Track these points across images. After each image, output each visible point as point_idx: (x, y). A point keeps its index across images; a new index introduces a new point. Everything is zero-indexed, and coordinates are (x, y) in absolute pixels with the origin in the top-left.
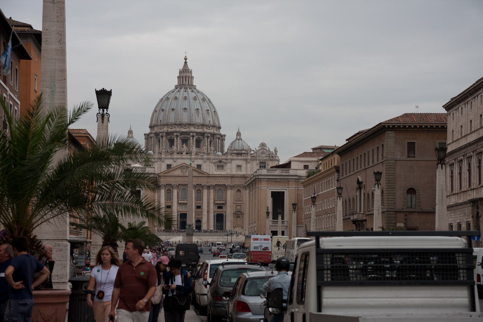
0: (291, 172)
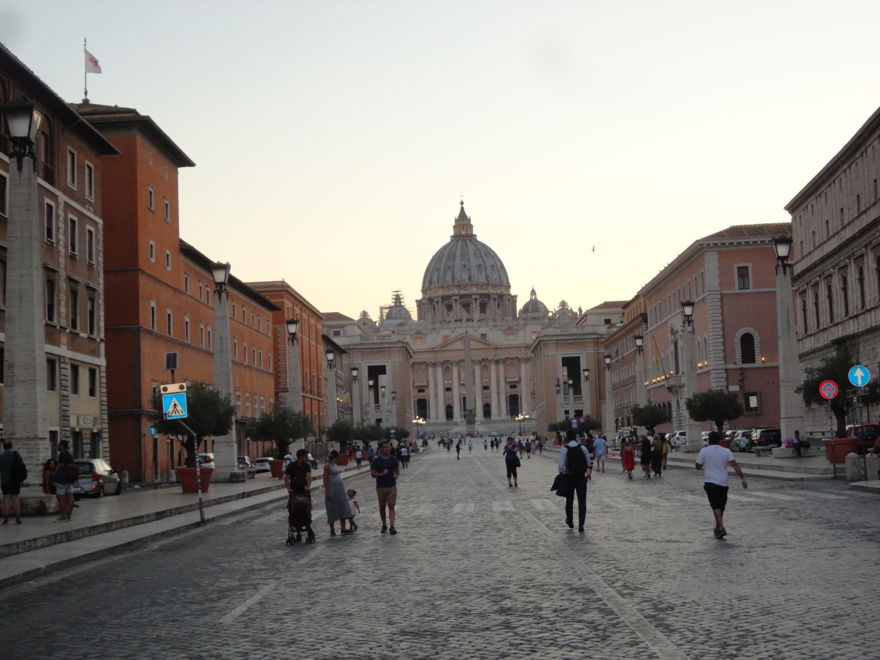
0: (588, 330)
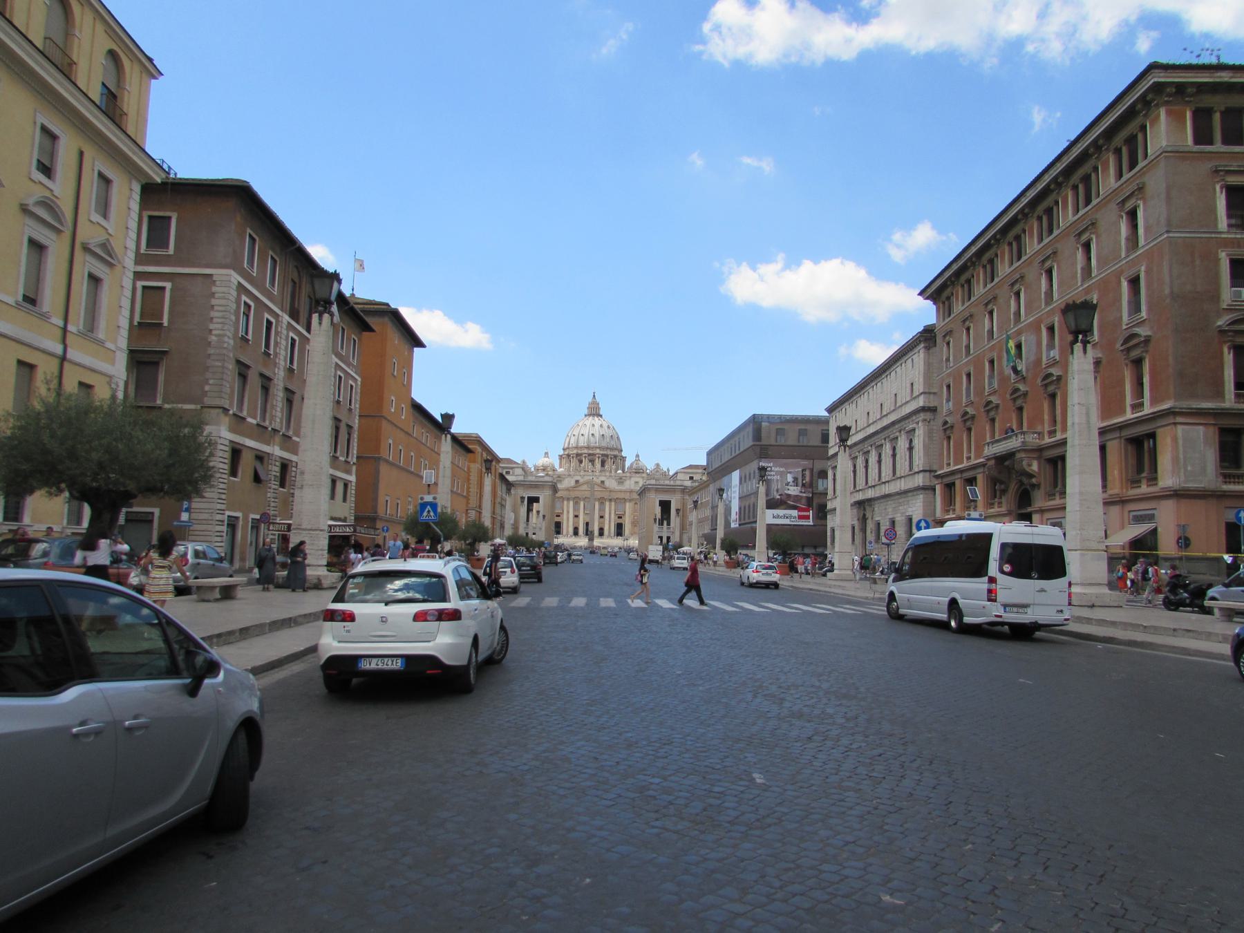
0: (678, 483)
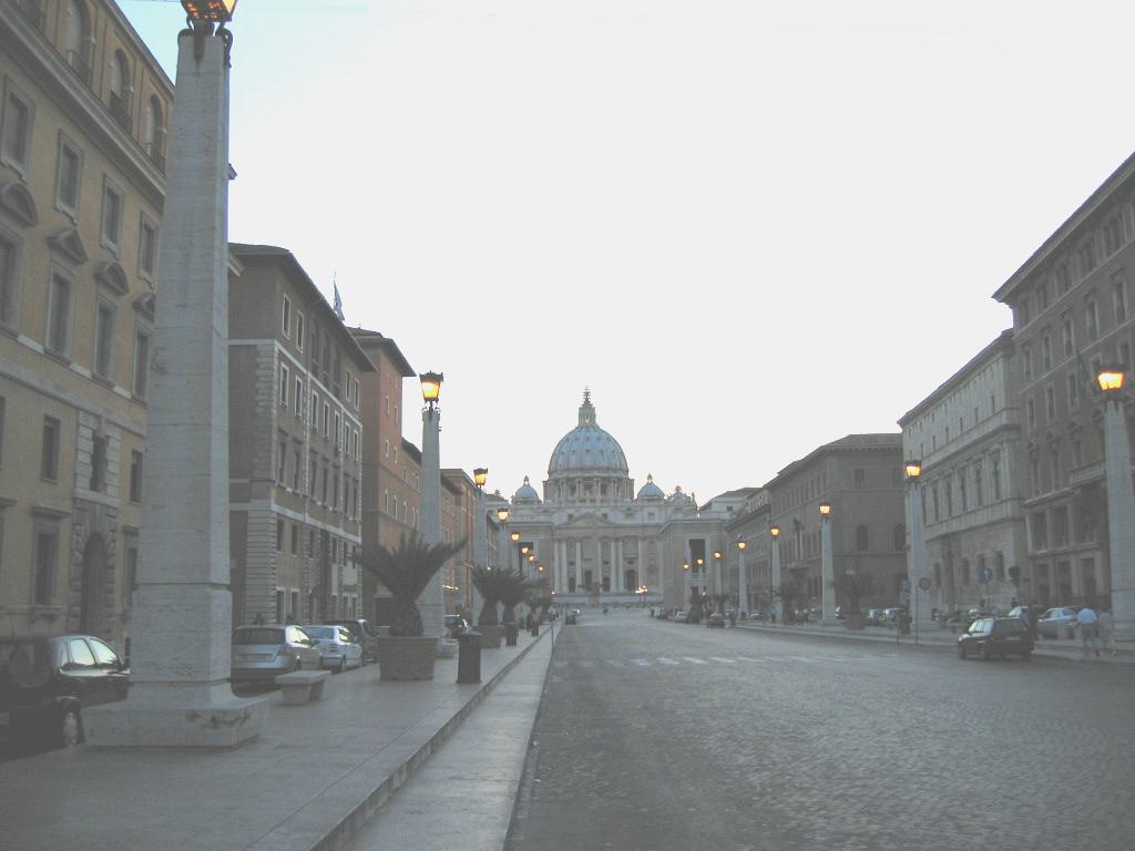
0: (714, 516)
